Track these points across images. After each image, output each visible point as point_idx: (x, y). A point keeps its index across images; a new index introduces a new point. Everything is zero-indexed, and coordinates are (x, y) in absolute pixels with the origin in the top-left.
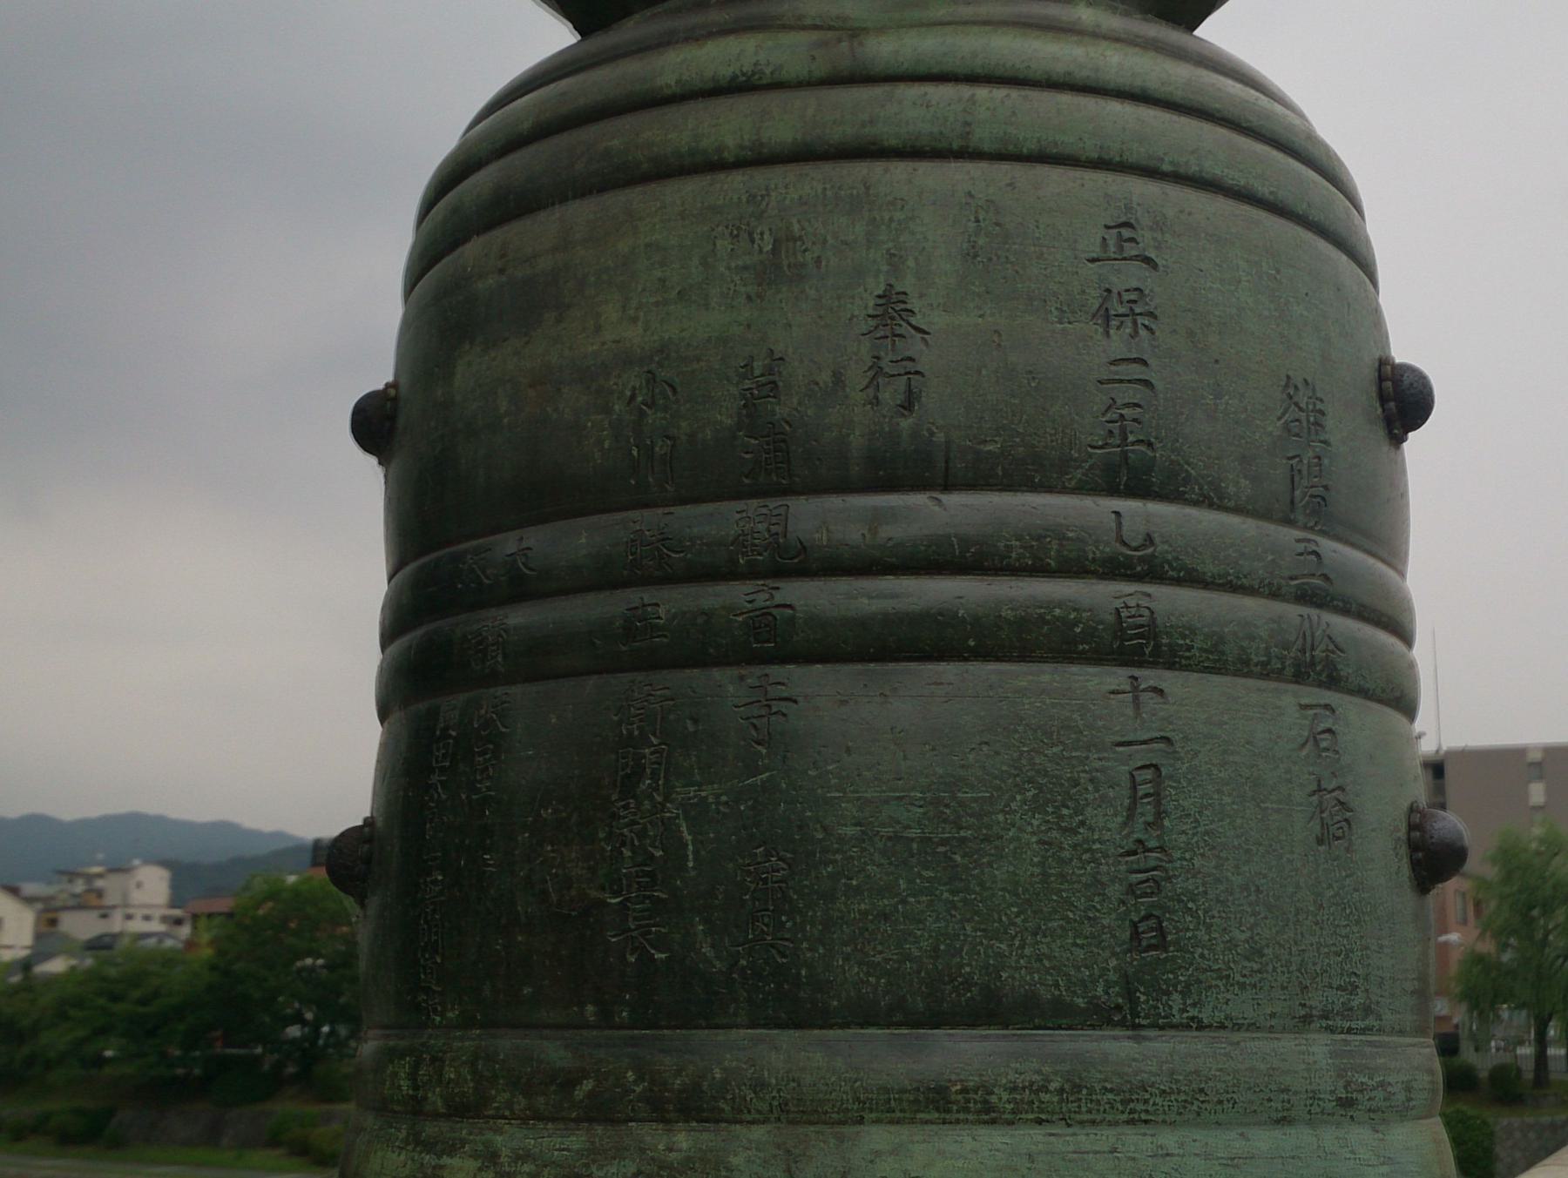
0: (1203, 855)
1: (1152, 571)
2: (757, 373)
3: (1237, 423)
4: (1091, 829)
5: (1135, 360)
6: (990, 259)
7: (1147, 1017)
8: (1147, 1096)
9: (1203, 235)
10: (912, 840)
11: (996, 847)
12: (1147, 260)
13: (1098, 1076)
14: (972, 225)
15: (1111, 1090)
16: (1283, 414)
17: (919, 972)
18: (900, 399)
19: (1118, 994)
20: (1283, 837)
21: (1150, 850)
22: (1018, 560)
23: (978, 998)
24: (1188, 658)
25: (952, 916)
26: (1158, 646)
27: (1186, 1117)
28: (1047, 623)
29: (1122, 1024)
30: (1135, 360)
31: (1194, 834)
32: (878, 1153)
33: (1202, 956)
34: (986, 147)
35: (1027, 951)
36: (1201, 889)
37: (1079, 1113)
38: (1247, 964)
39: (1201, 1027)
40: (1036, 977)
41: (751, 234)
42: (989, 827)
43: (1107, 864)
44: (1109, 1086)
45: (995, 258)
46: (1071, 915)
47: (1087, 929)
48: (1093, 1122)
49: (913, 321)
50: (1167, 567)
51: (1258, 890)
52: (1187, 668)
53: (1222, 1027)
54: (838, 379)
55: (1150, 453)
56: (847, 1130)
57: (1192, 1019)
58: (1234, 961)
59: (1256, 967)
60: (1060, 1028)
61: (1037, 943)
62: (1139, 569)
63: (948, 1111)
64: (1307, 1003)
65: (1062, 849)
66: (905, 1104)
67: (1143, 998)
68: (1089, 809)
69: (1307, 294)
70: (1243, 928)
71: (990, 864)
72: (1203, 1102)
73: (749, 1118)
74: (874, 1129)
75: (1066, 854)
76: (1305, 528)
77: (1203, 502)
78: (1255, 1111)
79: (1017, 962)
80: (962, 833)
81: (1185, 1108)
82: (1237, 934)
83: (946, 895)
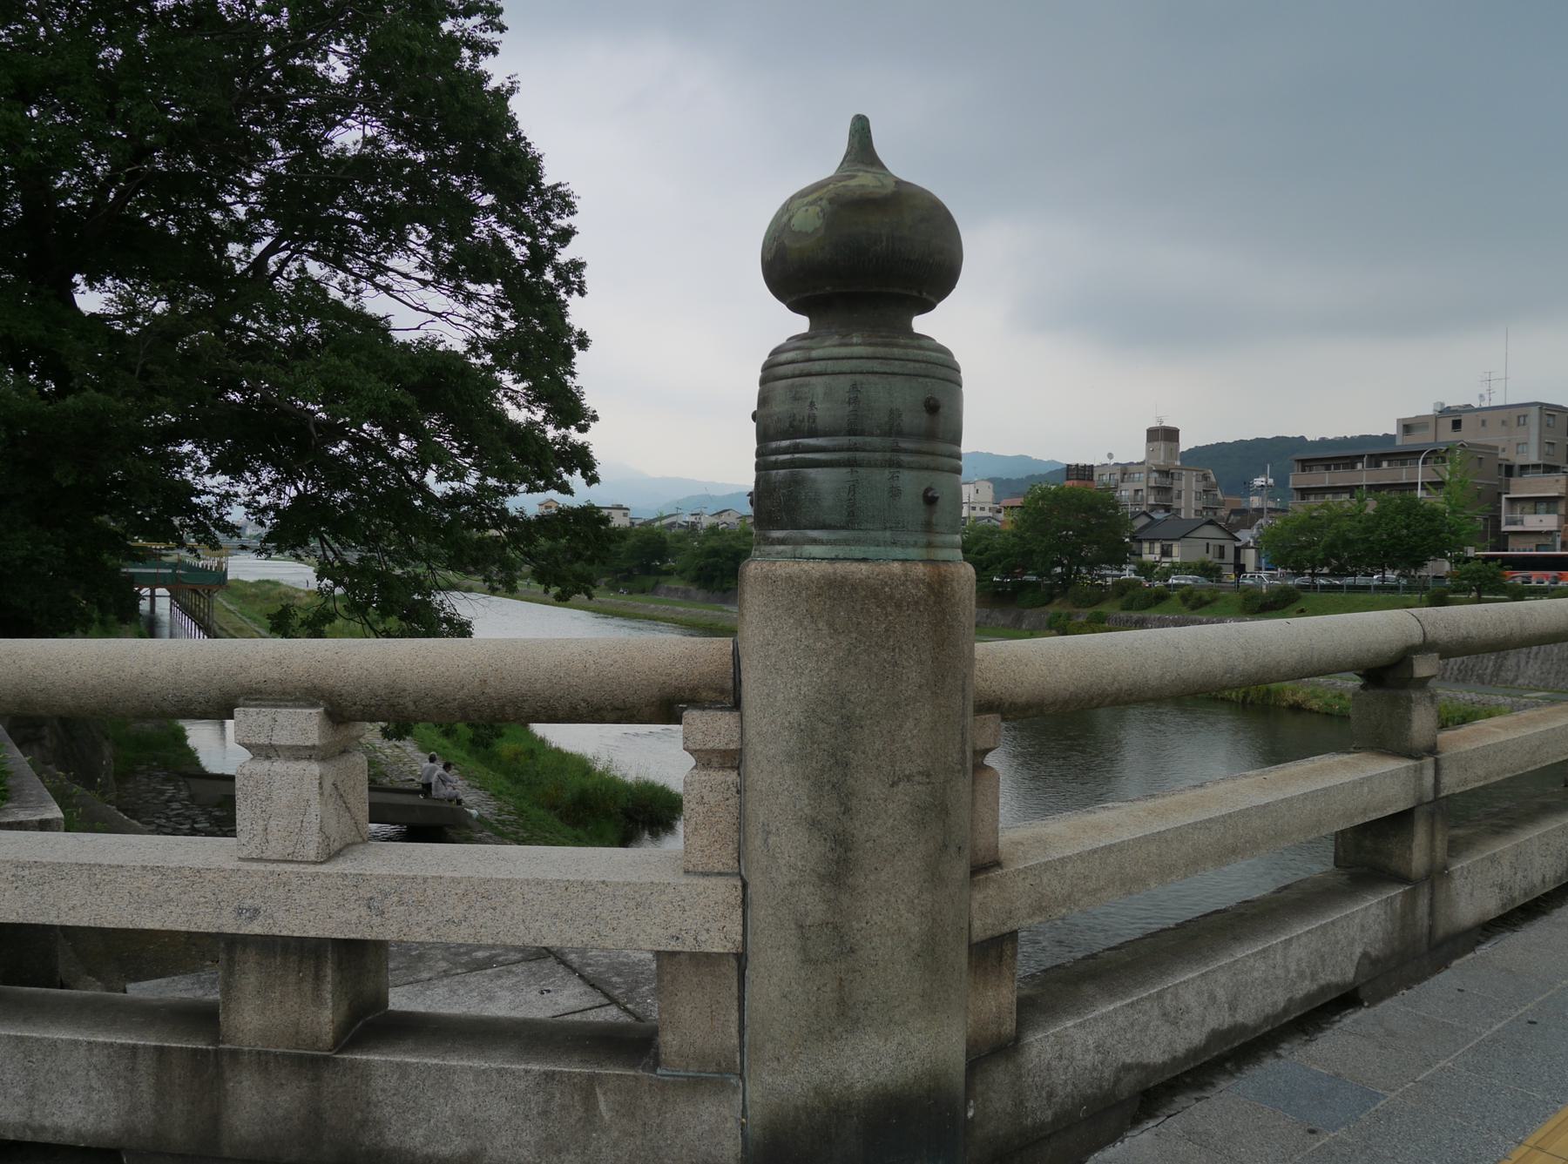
1: (857, 450)
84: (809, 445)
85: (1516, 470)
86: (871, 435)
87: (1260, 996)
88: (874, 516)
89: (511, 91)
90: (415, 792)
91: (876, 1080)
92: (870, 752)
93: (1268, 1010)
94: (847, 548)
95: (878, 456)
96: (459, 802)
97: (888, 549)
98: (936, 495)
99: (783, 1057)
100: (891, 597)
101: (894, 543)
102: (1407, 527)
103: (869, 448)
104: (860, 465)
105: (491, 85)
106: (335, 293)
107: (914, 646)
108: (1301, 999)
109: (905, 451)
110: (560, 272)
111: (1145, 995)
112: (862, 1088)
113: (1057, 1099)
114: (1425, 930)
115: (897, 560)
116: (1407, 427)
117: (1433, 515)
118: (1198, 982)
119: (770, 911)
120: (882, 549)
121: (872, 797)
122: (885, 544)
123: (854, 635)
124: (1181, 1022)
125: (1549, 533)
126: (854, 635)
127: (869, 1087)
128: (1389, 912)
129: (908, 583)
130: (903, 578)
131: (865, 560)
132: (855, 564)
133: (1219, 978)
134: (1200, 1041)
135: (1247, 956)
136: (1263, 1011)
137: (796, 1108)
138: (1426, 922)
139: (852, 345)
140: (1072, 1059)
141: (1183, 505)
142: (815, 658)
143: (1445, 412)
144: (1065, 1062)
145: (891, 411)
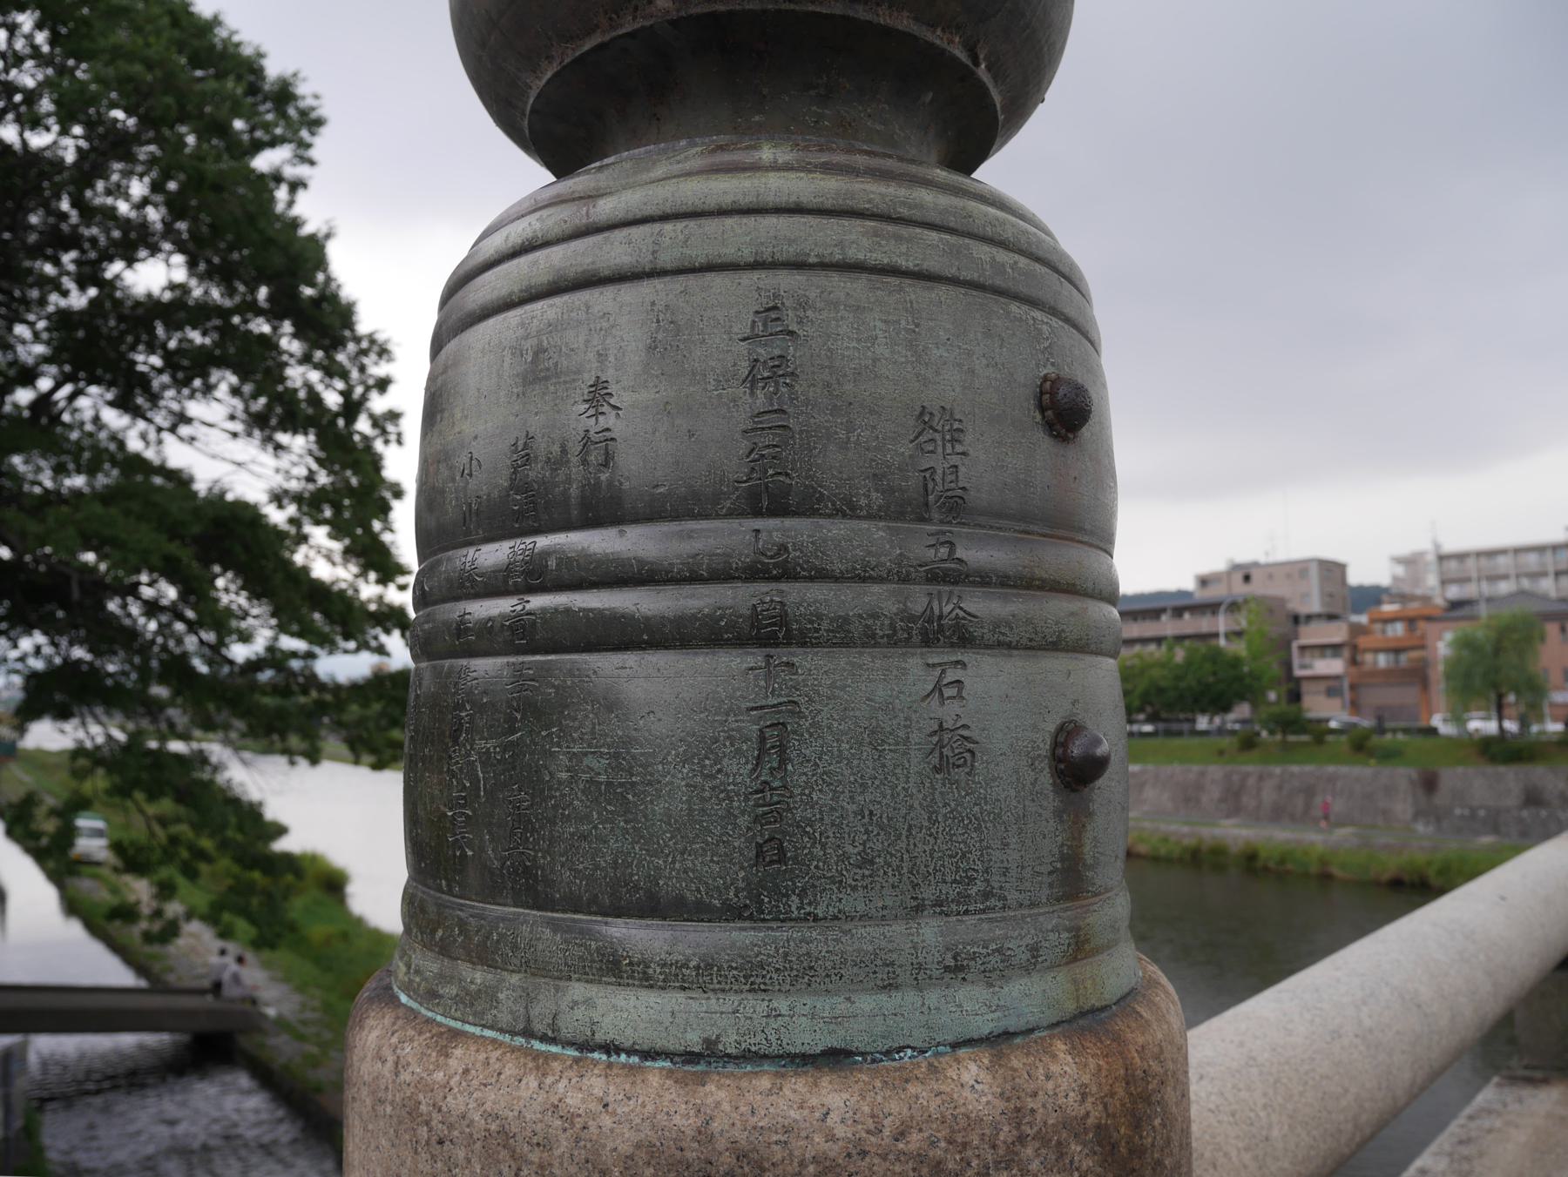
0: (820, 791)
1: (788, 574)
2: (520, 449)
3: (868, 450)
4: (727, 775)
5: (775, 411)
6: (666, 349)
7: (770, 913)
8: (765, 972)
9: (842, 307)
10: (601, 783)
11: (656, 789)
12: (791, 333)
13: (726, 957)
14: (654, 325)
15: (736, 968)
16: (917, 438)
17: (605, 878)
18: (601, 459)
19: (746, 897)
20: (898, 771)
21: (775, 789)
22: (679, 573)
23: (644, 898)
24: (816, 638)
25: (627, 839)
26: (789, 631)
27: (799, 987)
28: (699, 619)
29: (751, 918)
30: (775, 411)
31: (813, 775)
32: (576, 1003)
33: (817, 867)
34: (668, 266)
35: (677, 865)
36: (818, 816)
37: (712, 983)
38: (858, 871)
39: (816, 919)
40: (684, 885)
41: (521, 351)
42: (652, 775)
43: (739, 800)
44: (734, 965)
45: (669, 347)
46: (710, 839)
47: (722, 850)
48: (723, 990)
49: (612, 401)
50: (799, 569)
51: (871, 813)
52: (818, 645)
53: (835, 918)
54: (564, 451)
55: (788, 481)
56: (562, 983)
57: (809, 914)
58: (846, 869)
59: (867, 873)
60: (702, 921)
61: (684, 860)
62: (775, 572)
63: (622, 978)
64: (920, 896)
65: (704, 790)
66: (594, 970)
67: (766, 900)
68: (726, 760)
69: (948, 339)
70: (857, 844)
71: (652, 802)
72: (812, 976)
73: (511, 968)
74: (577, 985)
75: (707, 794)
76: (942, 522)
77: (837, 514)
78: (861, 981)
79: (670, 873)
80: (634, 779)
81: (797, 981)
82: (849, 849)
83: (622, 824)
84: (566, 560)
85: (1302, 620)
86: (847, 509)
88: (866, 861)
89: (328, 236)
90: (201, 992)
94: (756, 1006)
95: (880, 598)
96: (254, 1002)
97: (933, 997)
98: (1100, 751)
101: (956, 969)
102: (1215, 673)
103: (838, 567)
104: (804, 640)
105: (306, 230)
106: (134, 444)
109: (984, 580)
110: (377, 422)
115: (970, 1042)
116: (1204, 582)
117: (1236, 662)
120: (907, 999)
122: (921, 977)
125: (1337, 678)
131: (836, 1058)
132: (797, 1085)
139: (755, 168)
143: (1236, 567)
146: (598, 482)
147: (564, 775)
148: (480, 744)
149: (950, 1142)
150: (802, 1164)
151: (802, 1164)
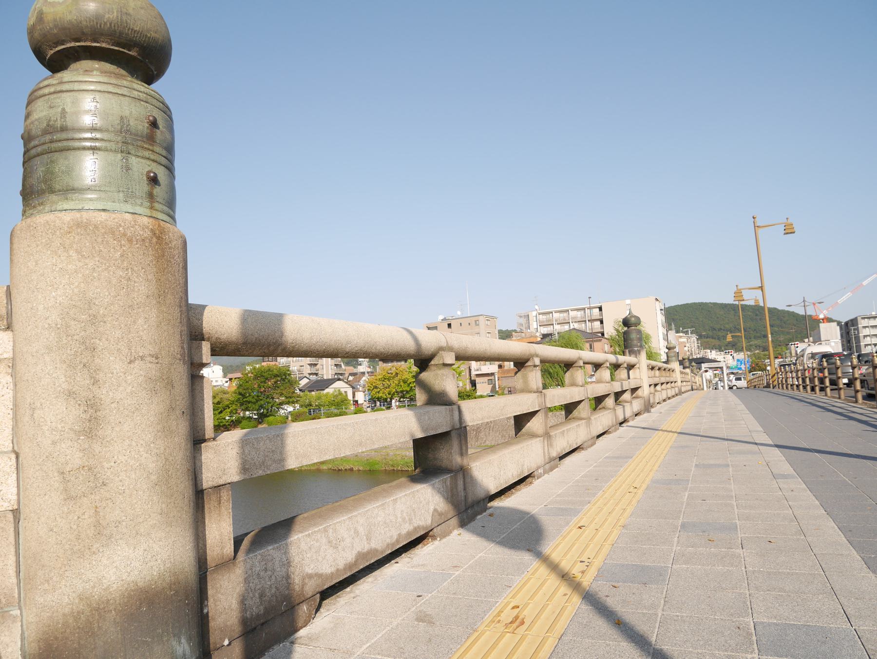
87: (383, 532)
91: (128, 579)
92: (112, 340)
93: (388, 541)
97: (122, 205)
99: (51, 578)
100: (124, 235)
107: (142, 268)
108: (405, 534)
111: (316, 529)
112: (118, 587)
113: (266, 598)
114: (463, 498)
118: (347, 522)
119: (38, 468)
121: (115, 372)
123: (97, 259)
124: (340, 547)
126: (97, 259)
127: (122, 586)
128: (445, 486)
129: (137, 227)
130: (132, 223)
133: (359, 520)
134: (352, 559)
135: (374, 508)
136: (385, 541)
137: (64, 615)
138: (462, 494)
140: (274, 570)
141: (325, 372)
142: (67, 276)
144: (269, 573)
145: (122, 118)
146: (63, 125)
147: (58, 171)
148: (41, 169)
149: (122, 221)
150: (97, 221)
151: (97, 221)
